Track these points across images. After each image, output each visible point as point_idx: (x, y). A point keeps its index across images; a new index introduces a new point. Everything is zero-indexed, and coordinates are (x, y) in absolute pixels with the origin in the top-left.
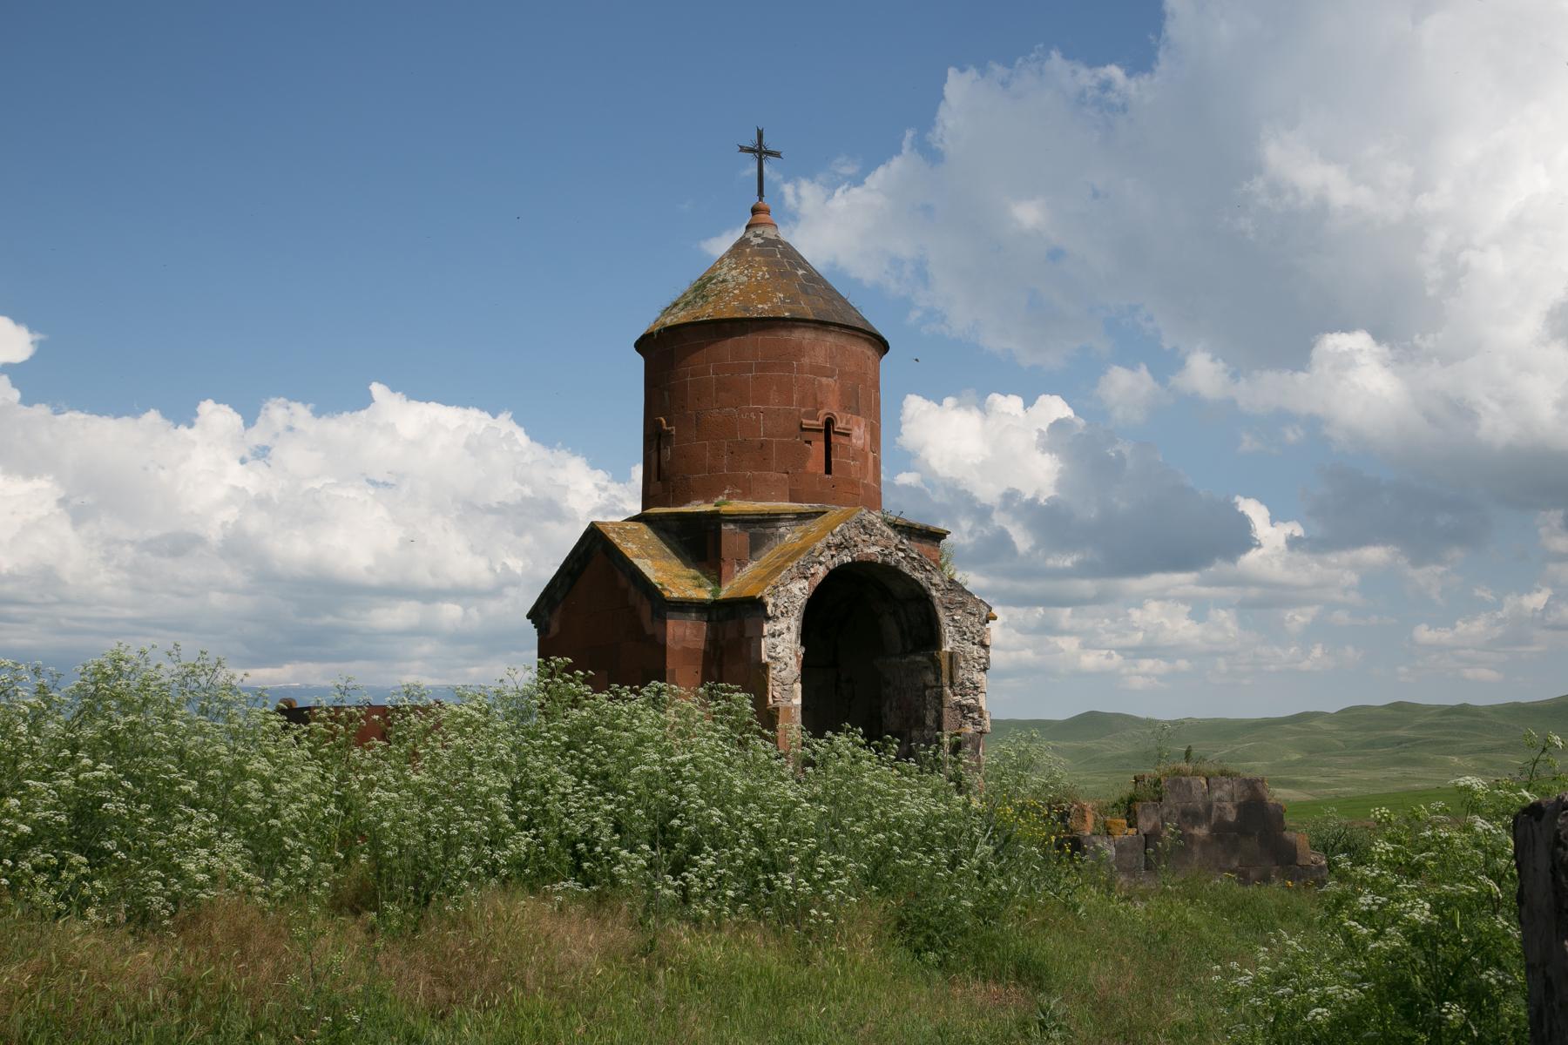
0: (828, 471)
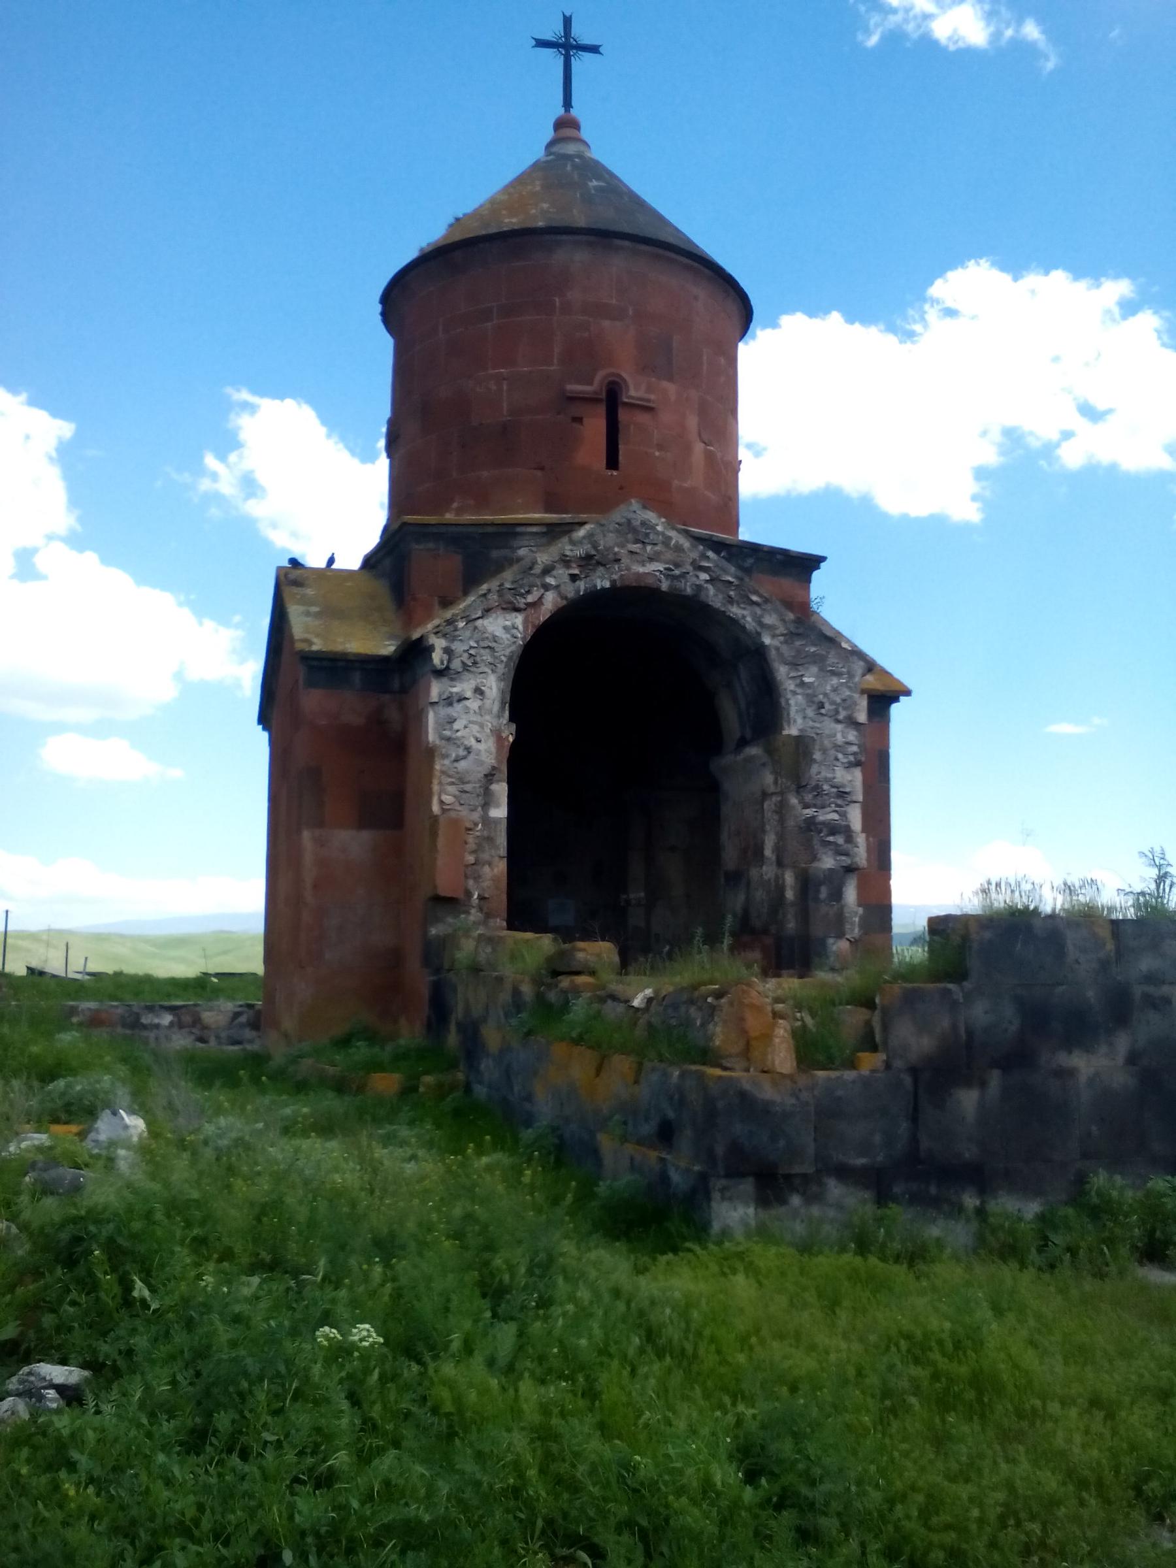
0: (612, 462)
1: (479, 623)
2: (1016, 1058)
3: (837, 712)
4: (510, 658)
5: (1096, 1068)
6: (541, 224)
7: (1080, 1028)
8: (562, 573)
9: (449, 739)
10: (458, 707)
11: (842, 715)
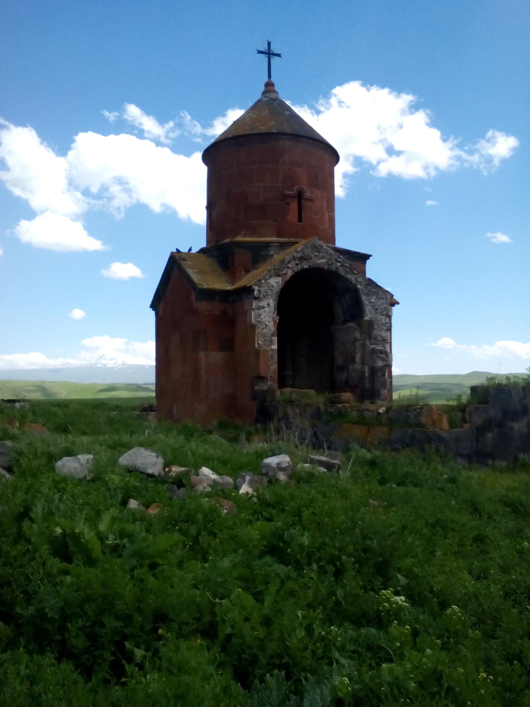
0: (300, 220)
1: (268, 281)
2: (501, 424)
3: (382, 312)
4: (277, 293)
5: (519, 426)
6: (275, 131)
7: (515, 416)
8: (293, 263)
9: (259, 322)
10: (262, 311)
11: (384, 313)
